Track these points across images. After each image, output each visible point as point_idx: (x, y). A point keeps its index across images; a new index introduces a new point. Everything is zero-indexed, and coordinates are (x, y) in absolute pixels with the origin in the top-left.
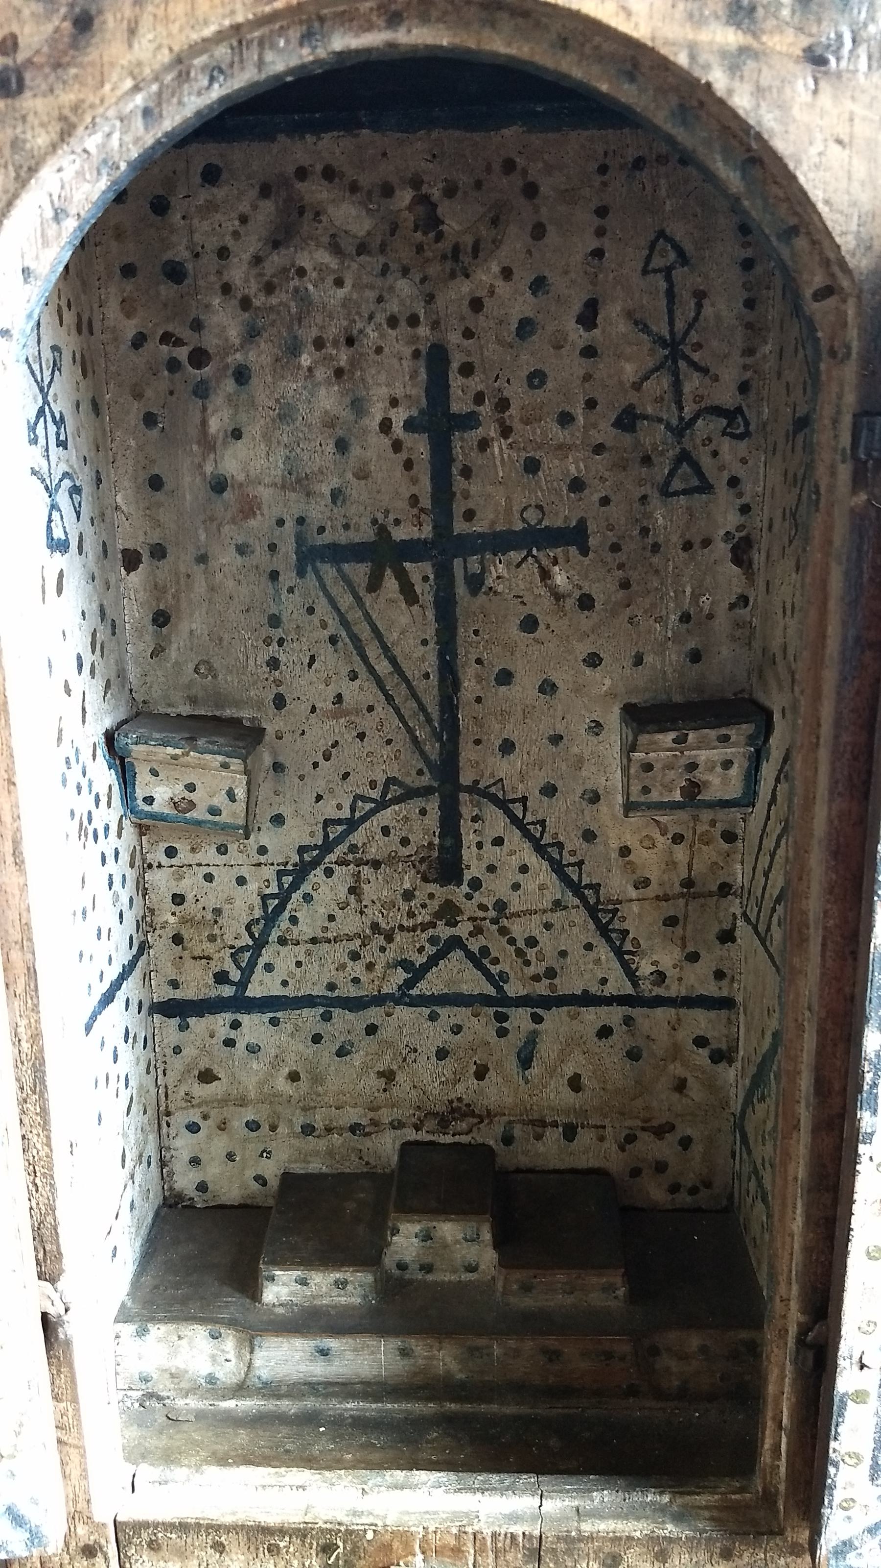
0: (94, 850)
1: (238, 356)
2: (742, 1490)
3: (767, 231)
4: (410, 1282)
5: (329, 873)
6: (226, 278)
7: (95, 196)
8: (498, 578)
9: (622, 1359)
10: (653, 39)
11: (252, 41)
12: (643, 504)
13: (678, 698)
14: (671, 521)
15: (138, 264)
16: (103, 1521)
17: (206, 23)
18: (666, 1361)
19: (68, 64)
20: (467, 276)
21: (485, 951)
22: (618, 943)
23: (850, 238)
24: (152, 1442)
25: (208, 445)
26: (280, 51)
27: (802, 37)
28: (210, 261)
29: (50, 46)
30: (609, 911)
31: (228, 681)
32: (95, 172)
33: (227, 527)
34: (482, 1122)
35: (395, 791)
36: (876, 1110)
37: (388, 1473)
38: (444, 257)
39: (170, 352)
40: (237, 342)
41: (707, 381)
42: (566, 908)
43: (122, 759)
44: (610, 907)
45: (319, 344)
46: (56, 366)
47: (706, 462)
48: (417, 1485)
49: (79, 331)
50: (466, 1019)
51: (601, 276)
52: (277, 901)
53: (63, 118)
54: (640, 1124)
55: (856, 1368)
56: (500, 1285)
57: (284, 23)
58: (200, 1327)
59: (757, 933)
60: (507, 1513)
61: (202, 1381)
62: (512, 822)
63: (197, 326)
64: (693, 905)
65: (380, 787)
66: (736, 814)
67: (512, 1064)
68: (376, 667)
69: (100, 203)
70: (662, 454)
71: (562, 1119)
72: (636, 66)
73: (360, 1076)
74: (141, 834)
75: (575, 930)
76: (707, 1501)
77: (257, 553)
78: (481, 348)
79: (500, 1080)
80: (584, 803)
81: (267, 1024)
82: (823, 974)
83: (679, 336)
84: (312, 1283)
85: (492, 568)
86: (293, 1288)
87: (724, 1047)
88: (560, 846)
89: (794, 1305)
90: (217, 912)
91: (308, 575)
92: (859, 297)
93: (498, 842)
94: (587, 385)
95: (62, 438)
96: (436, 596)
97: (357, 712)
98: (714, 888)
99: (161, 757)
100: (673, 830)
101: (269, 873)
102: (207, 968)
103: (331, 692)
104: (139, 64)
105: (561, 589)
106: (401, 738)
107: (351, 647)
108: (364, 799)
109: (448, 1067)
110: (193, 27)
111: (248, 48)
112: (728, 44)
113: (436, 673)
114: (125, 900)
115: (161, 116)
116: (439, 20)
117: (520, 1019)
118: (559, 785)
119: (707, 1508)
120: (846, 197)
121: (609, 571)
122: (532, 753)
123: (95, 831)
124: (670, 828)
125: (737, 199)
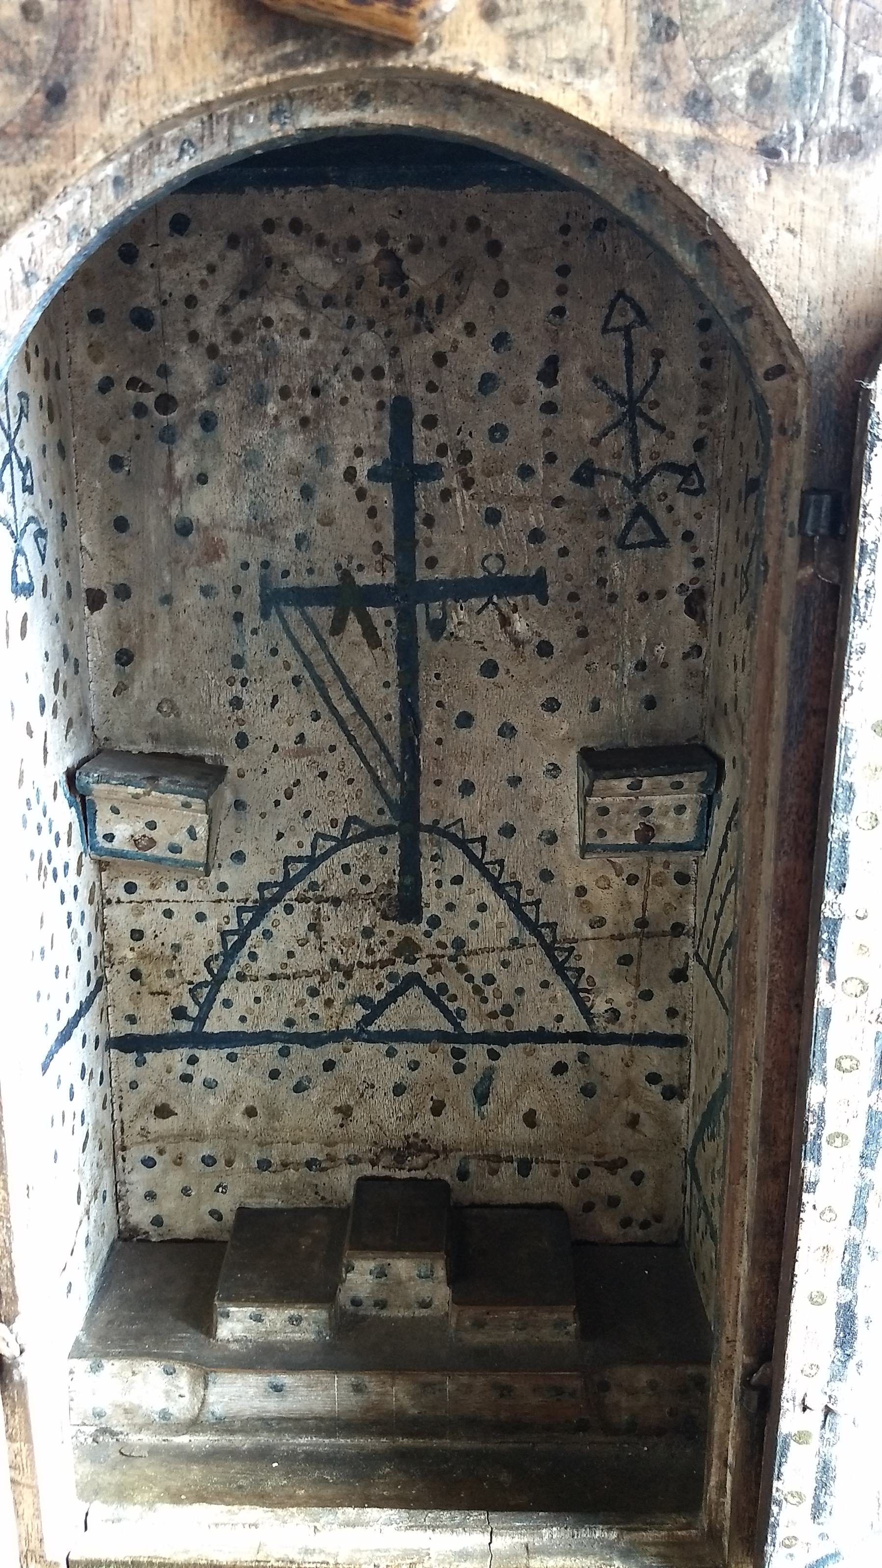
0: (53, 889)
1: (204, 403)
2: (688, 1527)
3: (721, 312)
4: (364, 1318)
5: (289, 909)
6: (193, 326)
7: (65, 262)
8: (459, 623)
9: (573, 1394)
10: (612, 128)
11: (222, 116)
12: (601, 556)
13: (633, 743)
14: (628, 573)
15: (106, 310)
16: (55, 1560)
17: (177, 100)
18: (614, 1396)
19: (41, 135)
20: (431, 331)
21: (443, 988)
22: (574, 981)
23: (800, 322)
24: (108, 1478)
25: (174, 488)
26: (249, 127)
27: (756, 130)
28: (177, 308)
29: (22, 117)
30: (565, 950)
31: (191, 720)
32: (66, 239)
33: (192, 569)
34: (438, 1157)
35: (356, 829)
36: (819, 1160)
37: (340, 1511)
38: (409, 311)
39: (137, 397)
40: (204, 389)
41: (664, 438)
42: (523, 946)
43: (83, 797)
44: (566, 946)
45: (285, 393)
46: (23, 413)
47: (661, 516)
48: (368, 1523)
49: (47, 376)
50: (423, 1055)
51: (562, 334)
52: (236, 937)
53: (34, 187)
54: (593, 1159)
55: (799, 1409)
56: (453, 1321)
57: (254, 100)
58: (154, 1363)
59: (708, 973)
60: (457, 1550)
61: (156, 1416)
62: (471, 862)
63: (164, 372)
64: (648, 944)
65: (341, 825)
66: (689, 857)
67: (468, 1100)
68: (339, 708)
69: (70, 267)
70: (619, 507)
71: (517, 1154)
72: (596, 151)
73: (317, 1112)
74: (101, 870)
75: (532, 968)
76: (654, 1538)
77: (222, 595)
78: (444, 401)
79: (456, 1116)
80: (542, 843)
81: (224, 1059)
82: (769, 1026)
83: (637, 393)
84: (266, 1320)
85: (454, 614)
86: (247, 1325)
87: (676, 1084)
88: (518, 885)
89: (740, 1347)
90: (176, 947)
91: (272, 617)
92: (808, 378)
93: (457, 880)
94: (547, 439)
95: (28, 483)
96: (398, 641)
97: (319, 751)
98: (668, 928)
99: (121, 795)
100: (628, 871)
101: (229, 909)
102: (165, 1003)
103: (293, 732)
104: (111, 137)
105: (521, 636)
106: (362, 778)
107: (314, 688)
108: (325, 837)
109: (405, 1103)
110: (164, 103)
111: (218, 123)
112: (684, 135)
113: (398, 714)
114: (83, 937)
115: (132, 186)
116: (405, 102)
117: (477, 1055)
118: (518, 825)
119: (654, 1544)
120: (797, 283)
121: (567, 619)
122: (491, 794)
123: (55, 870)
124: (625, 870)
125: (693, 281)
